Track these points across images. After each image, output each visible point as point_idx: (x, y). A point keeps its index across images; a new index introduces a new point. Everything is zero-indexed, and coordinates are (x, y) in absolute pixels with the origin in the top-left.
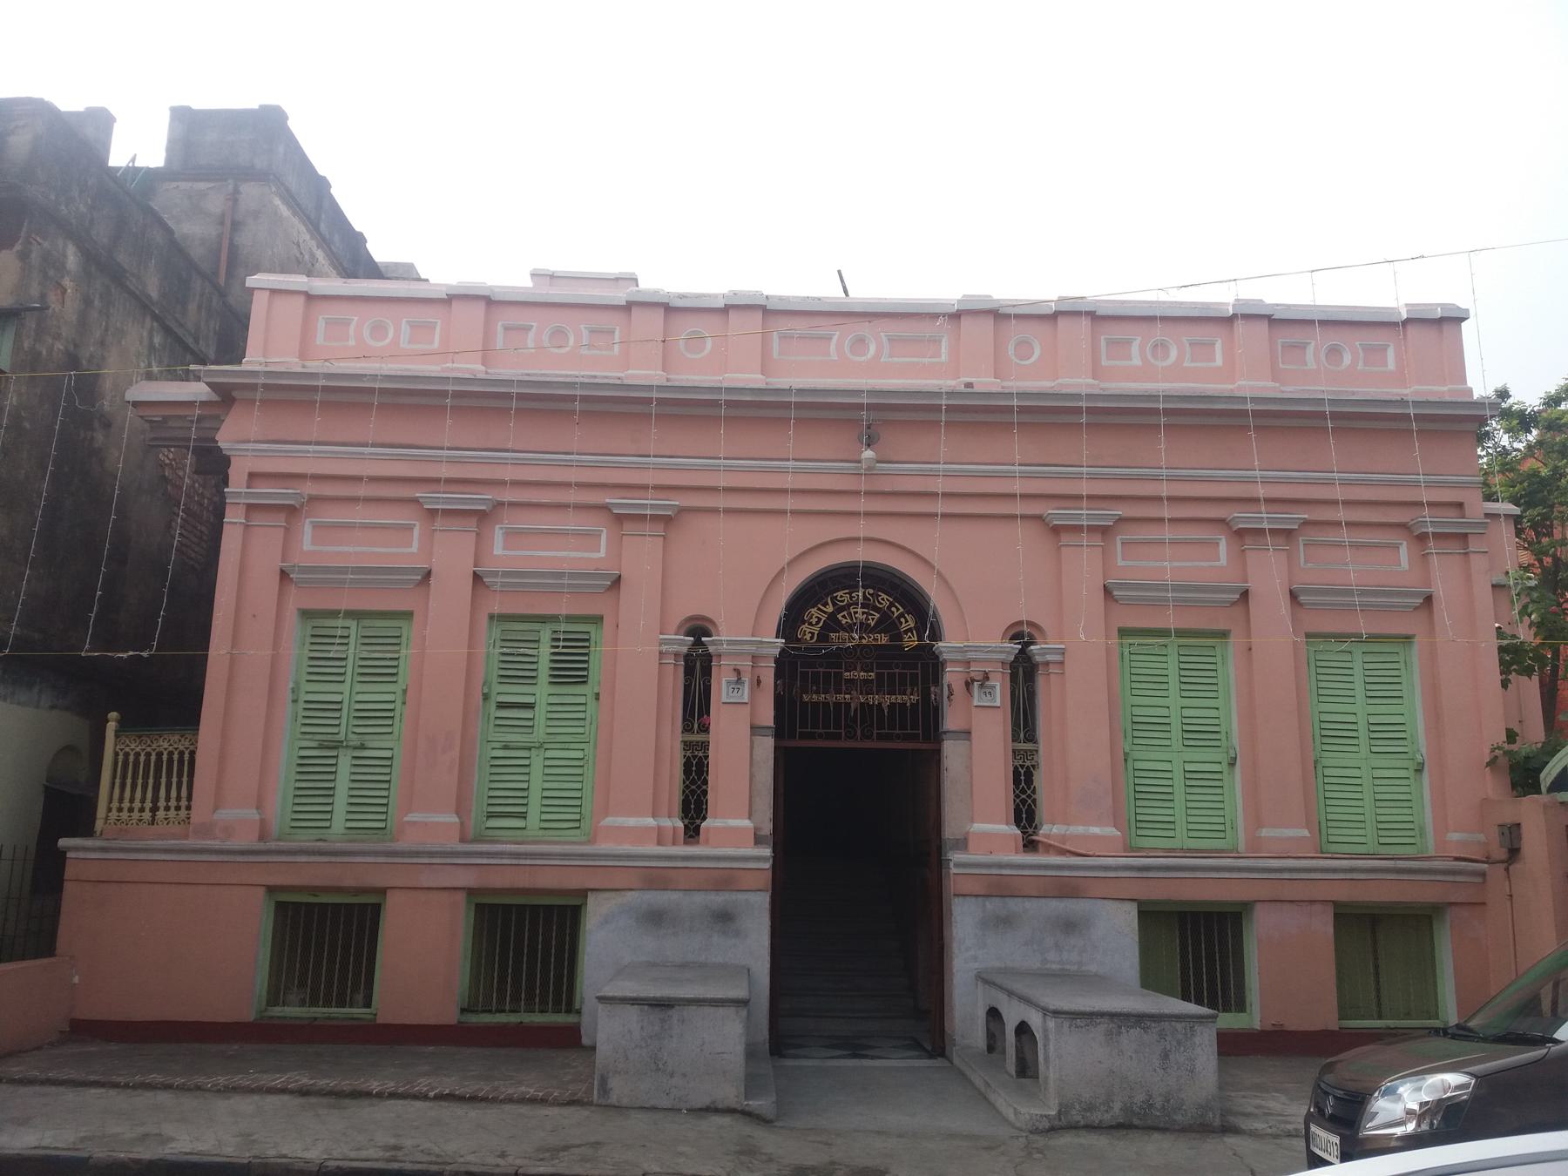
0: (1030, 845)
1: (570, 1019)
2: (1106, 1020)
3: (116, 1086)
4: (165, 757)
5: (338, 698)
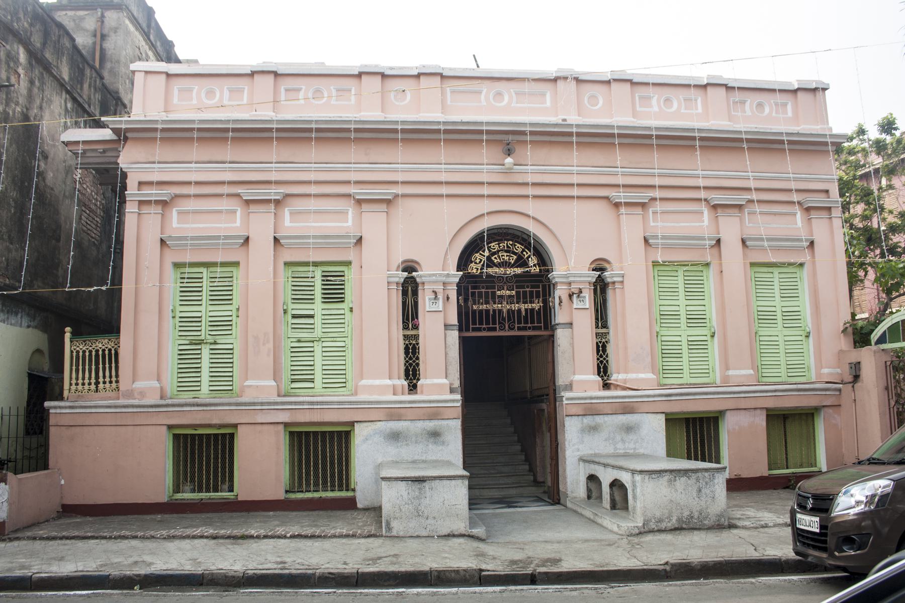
0: (606, 386)
1: (350, 494)
2: (668, 474)
3: (105, 538)
4: (100, 353)
5: (199, 314)
